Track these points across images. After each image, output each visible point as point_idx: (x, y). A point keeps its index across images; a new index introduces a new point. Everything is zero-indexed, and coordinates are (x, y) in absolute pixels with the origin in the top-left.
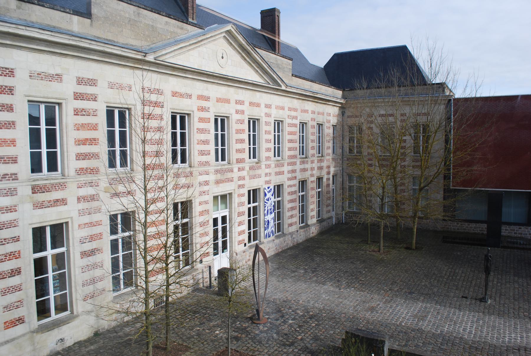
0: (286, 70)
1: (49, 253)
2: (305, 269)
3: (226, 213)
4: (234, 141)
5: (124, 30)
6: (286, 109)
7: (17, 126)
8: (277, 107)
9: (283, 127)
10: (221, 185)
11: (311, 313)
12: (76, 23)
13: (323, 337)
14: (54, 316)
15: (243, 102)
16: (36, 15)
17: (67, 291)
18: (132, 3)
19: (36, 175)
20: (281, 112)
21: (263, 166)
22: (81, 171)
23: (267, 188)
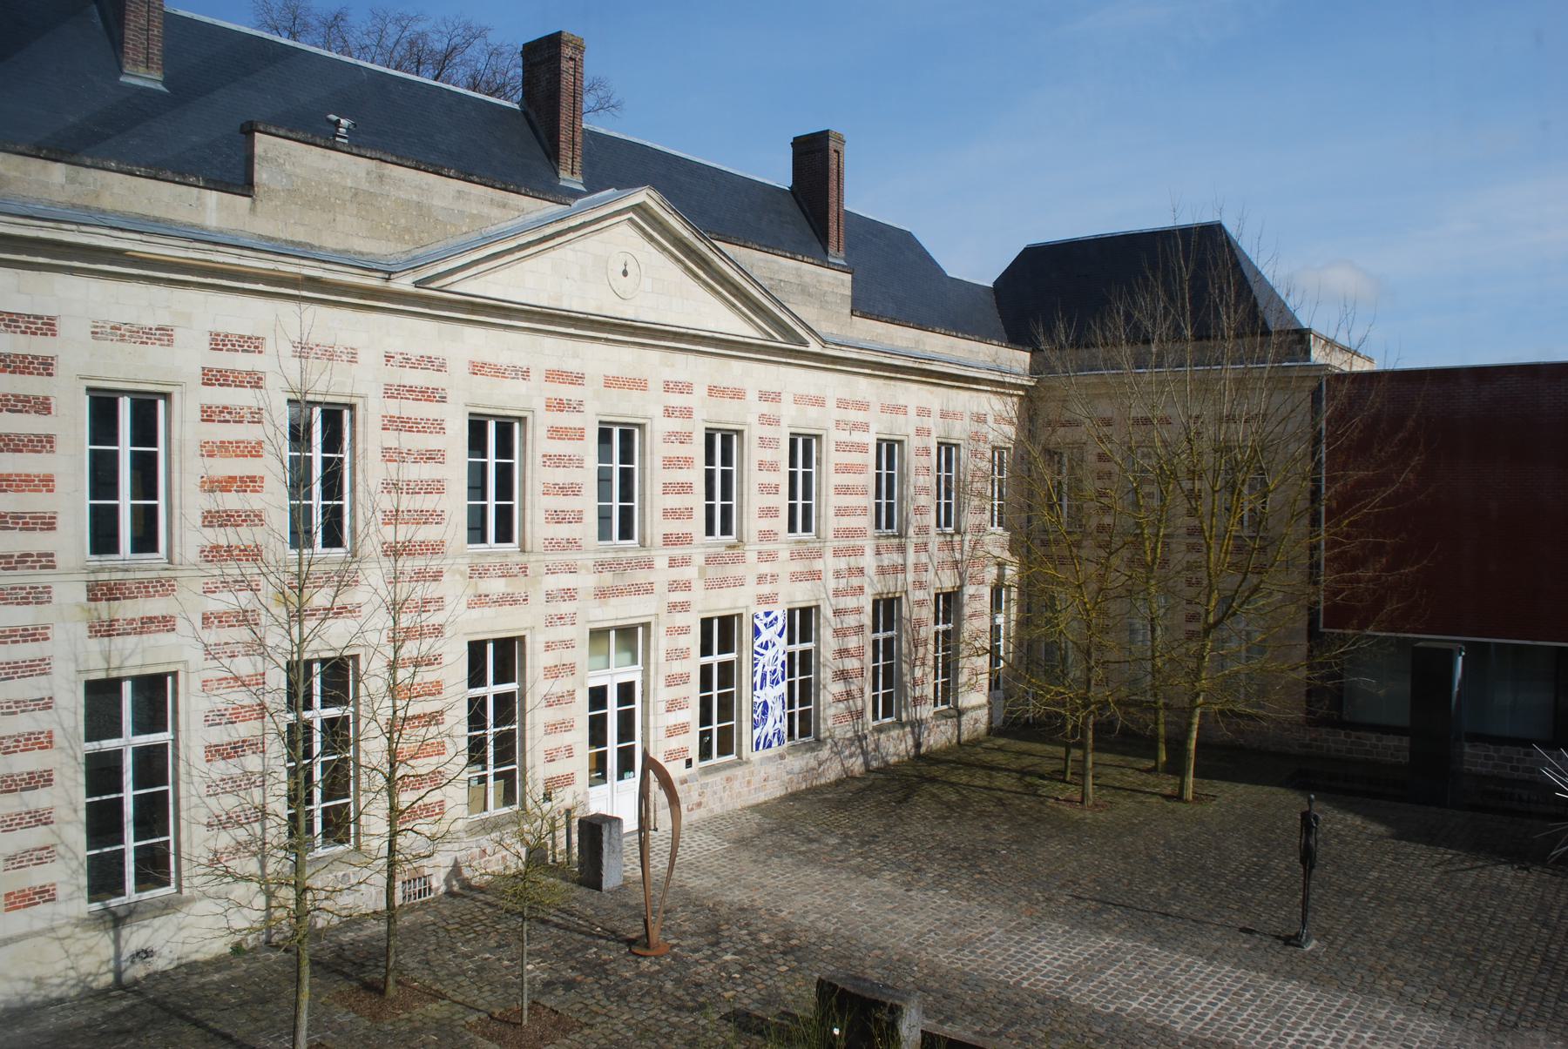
0: (830, 298)
1: (128, 742)
2: (847, 836)
3: (633, 674)
4: (659, 488)
5: (339, 218)
6: (831, 404)
7: (58, 447)
8: (799, 400)
9: (820, 451)
10: (613, 601)
11: (794, 942)
12: (213, 209)
13: (789, 998)
14: (131, 893)
15: (690, 386)
16: (112, 194)
17: (171, 837)
18: (363, 152)
19: (108, 560)
20: (813, 412)
21: (751, 556)
22: (214, 554)
23: (761, 615)
